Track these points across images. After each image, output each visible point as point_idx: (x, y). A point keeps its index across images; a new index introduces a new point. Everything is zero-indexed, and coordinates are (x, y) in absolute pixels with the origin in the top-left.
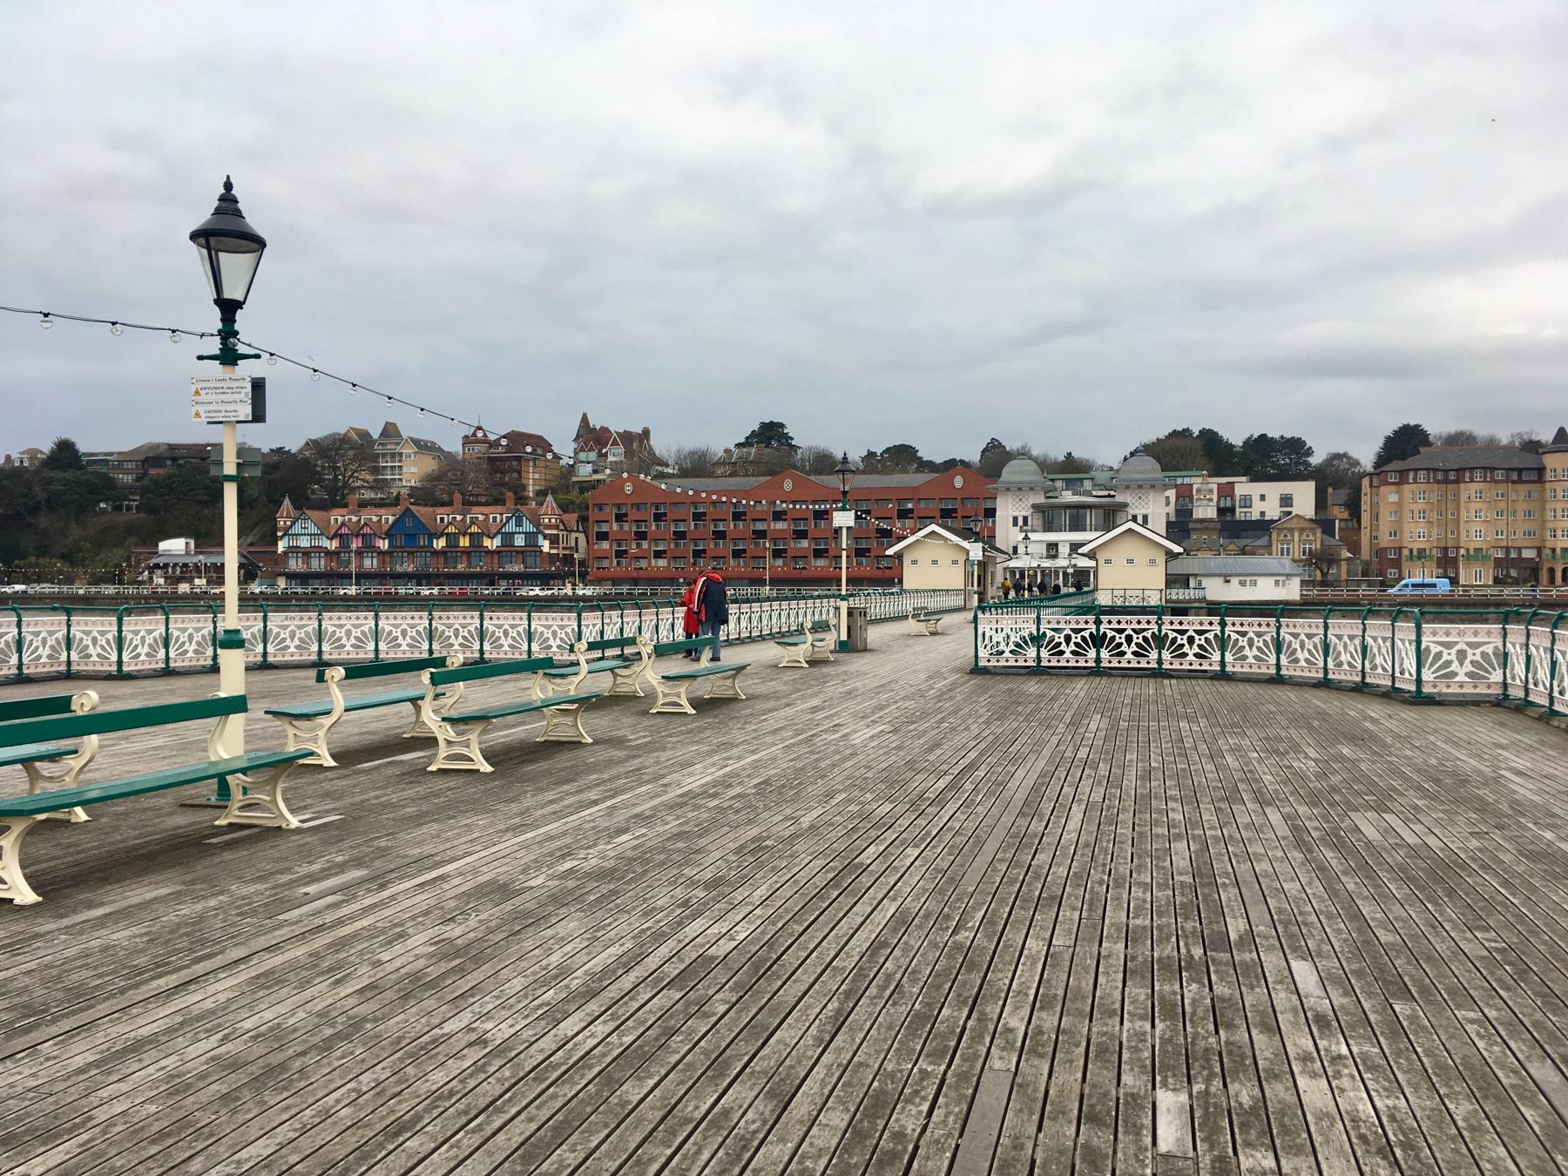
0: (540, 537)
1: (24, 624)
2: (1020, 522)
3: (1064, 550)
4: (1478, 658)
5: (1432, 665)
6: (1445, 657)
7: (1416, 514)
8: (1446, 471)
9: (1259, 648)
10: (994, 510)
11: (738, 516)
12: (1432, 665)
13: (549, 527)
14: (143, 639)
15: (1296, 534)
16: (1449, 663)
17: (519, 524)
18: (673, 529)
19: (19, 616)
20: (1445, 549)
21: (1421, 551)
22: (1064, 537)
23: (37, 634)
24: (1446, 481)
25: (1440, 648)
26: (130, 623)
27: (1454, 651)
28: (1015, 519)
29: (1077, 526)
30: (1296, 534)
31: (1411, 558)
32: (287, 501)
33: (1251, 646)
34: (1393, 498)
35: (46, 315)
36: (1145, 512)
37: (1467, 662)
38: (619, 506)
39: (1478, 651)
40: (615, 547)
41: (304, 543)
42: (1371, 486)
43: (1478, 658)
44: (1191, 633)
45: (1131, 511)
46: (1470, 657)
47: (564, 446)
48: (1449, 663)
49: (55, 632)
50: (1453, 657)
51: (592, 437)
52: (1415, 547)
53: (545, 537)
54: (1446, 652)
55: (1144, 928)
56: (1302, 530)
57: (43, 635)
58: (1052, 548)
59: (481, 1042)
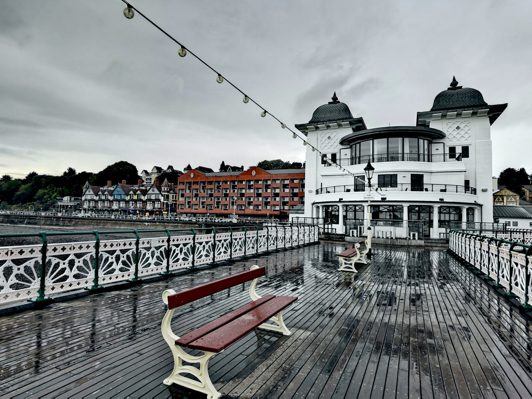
4: (22, 271)
5: (52, 273)
6: (61, 266)
9: (57, 265)
12: (52, 273)
13: (164, 192)
14: (181, 249)
16: (63, 270)
25: (58, 260)
27: (114, 256)
32: (166, 180)
33: (181, 252)
37: (75, 268)
39: (22, 267)
40: (248, 200)
41: (153, 197)
43: (22, 271)
44: (118, 252)
45: (449, 142)
46: (77, 264)
47: (216, 169)
48: (63, 270)
49: (227, 240)
50: (66, 265)
51: (224, 168)
53: (162, 195)
54: (62, 262)
57: (181, 246)
59: (499, 327)
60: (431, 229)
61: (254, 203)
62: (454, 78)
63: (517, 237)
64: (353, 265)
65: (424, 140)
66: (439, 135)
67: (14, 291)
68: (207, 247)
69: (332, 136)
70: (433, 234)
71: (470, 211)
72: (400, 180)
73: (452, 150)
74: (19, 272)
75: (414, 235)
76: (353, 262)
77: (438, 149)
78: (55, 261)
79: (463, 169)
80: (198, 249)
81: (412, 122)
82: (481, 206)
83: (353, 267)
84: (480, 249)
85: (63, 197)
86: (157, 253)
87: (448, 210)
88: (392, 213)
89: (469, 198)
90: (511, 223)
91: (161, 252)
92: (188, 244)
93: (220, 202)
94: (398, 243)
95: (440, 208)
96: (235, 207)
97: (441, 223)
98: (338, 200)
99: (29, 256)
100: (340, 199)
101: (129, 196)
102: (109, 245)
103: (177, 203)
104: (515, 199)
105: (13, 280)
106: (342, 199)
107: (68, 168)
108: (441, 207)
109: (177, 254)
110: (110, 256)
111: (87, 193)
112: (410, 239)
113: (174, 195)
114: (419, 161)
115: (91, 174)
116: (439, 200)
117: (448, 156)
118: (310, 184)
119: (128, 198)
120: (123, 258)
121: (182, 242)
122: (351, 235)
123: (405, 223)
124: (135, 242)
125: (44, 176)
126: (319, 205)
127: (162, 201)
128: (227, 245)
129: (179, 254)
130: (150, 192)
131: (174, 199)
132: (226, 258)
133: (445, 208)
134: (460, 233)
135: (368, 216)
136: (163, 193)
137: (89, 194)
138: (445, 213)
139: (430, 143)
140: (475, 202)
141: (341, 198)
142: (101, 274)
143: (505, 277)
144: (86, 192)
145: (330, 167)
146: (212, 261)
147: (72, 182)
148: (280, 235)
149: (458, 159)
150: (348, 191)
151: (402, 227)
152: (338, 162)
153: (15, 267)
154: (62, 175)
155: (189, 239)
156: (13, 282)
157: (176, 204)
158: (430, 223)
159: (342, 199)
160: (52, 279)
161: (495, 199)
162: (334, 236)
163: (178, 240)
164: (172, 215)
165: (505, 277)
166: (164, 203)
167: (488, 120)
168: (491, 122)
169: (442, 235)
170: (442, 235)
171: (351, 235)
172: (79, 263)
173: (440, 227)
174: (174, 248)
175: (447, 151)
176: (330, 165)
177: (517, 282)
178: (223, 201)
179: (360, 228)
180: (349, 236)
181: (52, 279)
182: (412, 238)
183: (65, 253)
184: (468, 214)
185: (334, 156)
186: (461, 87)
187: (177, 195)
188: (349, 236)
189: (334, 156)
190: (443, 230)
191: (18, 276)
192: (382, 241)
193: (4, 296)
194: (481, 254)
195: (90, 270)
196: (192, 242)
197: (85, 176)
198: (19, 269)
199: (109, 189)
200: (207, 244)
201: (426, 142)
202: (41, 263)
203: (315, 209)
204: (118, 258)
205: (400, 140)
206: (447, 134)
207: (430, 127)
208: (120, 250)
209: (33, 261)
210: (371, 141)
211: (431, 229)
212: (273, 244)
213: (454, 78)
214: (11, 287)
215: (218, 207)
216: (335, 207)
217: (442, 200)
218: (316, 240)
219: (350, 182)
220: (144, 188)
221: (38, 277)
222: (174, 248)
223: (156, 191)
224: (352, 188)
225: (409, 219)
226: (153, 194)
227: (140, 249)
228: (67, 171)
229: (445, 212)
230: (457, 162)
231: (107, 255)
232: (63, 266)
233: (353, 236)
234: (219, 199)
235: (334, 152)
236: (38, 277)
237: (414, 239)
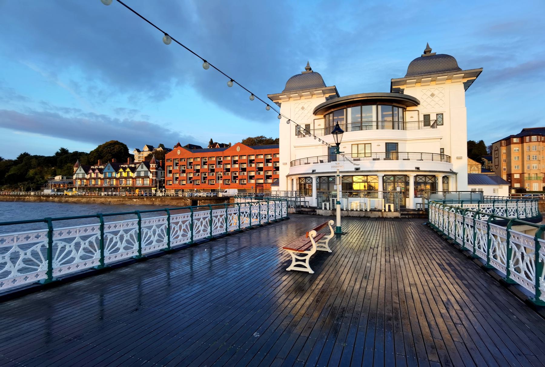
0: (149, 172)
1: (142, 222)
9: (64, 248)
10: (278, 167)
13: (153, 169)
14: (180, 226)
16: (70, 252)
17: (142, 168)
19: (140, 218)
23: (116, 233)
25: (64, 243)
26: (146, 221)
33: (154, 234)
35: (232, 80)
39: (29, 251)
43: (29, 256)
45: (423, 109)
46: (82, 246)
48: (70, 252)
50: (73, 247)
53: (151, 172)
57: (154, 227)
60: (407, 199)
61: (239, 178)
62: (428, 44)
66: (414, 102)
67: (22, 274)
68: (184, 227)
69: (305, 106)
71: (446, 179)
73: (427, 118)
74: (26, 257)
75: (389, 206)
77: (411, 115)
78: (60, 245)
79: (439, 136)
80: (196, 226)
81: (385, 90)
82: (456, 174)
83: (307, 264)
85: (55, 176)
86: (502, 211)
88: (366, 184)
89: (443, 166)
91: (186, 226)
92: (187, 221)
93: (206, 177)
94: (351, 214)
96: (221, 182)
98: (311, 172)
99: (36, 241)
100: (313, 171)
101: (119, 174)
102: (112, 226)
103: (166, 179)
105: (20, 264)
107: (60, 148)
108: (417, 175)
109: (177, 231)
110: (115, 237)
111: (78, 172)
112: (385, 211)
113: (163, 171)
114: (393, 128)
115: (82, 154)
116: (414, 169)
117: (422, 124)
118: (284, 155)
119: (118, 175)
120: (127, 237)
121: (486, 207)
122: (323, 209)
123: (380, 195)
124: (137, 222)
125: (36, 157)
126: (293, 177)
127: (151, 177)
128: (207, 223)
129: (179, 231)
130: (139, 169)
131: (163, 176)
132: (206, 236)
133: (421, 177)
135: (338, 188)
136: (152, 170)
137: (79, 172)
139: (404, 110)
140: (451, 170)
141: (314, 169)
142: (106, 253)
144: (77, 170)
145: (304, 138)
146: (190, 241)
147: (64, 161)
148: (255, 211)
149: (433, 127)
150: (322, 162)
151: (377, 197)
152: (312, 132)
153: (22, 253)
154: (54, 155)
155: (188, 217)
156: (20, 267)
157: (164, 180)
158: (405, 193)
160: (59, 262)
161: (471, 168)
162: (307, 210)
163: (177, 218)
164: (161, 191)
166: (152, 179)
171: (323, 209)
172: (84, 244)
173: (416, 196)
174: (496, 209)
175: (422, 118)
176: (304, 136)
178: (210, 176)
179: (333, 200)
180: (321, 208)
181: (59, 262)
182: (387, 210)
183: (71, 236)
184: (443, 182)
187: (166, 171)
188: (321, 208)
189: (308, 126)
190: (420, 200)
191: (25, 261)
192: (355, 214)
193: (13, 280)
195: (96, 251)
196: (190, 219)
197: (77, 155)
198: (26, 254)
199: (100, 167)
200: (184, 224)
202: (48, 247)
203: (290, 182)
204: (122, 238)
205: (374, 107)
207: (404, 93)
208: (124, 230)
209: (39, 246)
211: (407, 199)
212: (265, 218)
213: (428, 44)
214: (20, 271)
215: (205, 182)
216: (309, 179)
217: (418, 168)
218: (285, 215)
219: (323, 152)
220: (133, 166)
221: (46, 260)
222: (496, 209)
223: (145, 168)
224: (326, 159)
225: (383, 190)
226: (142, 170)
227: (105, 234)
228: (59, 151)
230: (432, 129)
231: (112, 236)
232: (70, 249)
233: (325, 209)
234: (205, 175)
235: (307, 123)
236: (46, 260)
237: (390, 210)
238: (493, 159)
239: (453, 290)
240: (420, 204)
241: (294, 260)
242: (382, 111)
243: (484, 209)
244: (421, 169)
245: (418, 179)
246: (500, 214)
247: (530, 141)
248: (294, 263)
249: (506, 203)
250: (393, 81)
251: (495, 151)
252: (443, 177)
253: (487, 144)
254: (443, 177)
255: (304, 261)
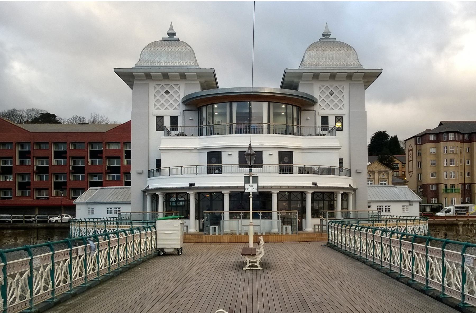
2: (167, 122)
3: (230, 160)
7: (449, 162)
8: (464, 134)
11: (94, 155)
15: (376, 175)
18: (107, 164)
20: (464, 185)
21: (453, 186)
22: (232, 143)
24: (463, 141)
28: (160, 119)
29: (246, 126)
30: (376, 175)
31: (446, 191)
34: (433, 151)
36: (338, 112)
38: (22, 144)
42: (416, 144)
45: (321, 110)
52: (449, 183)
55: (246, 113)
56: (380, 171)
58: (214, 161)
60: (303, 220)
63: (392, 225)
64: (258, 262)
65: (293, 106)
70: (306, 227)
71: (345, 196)
72: (266, 159)
76: (258, 260)
83: (258, 265)
84: (373, 241)
87: (321, 196)
90: (384, 208)
95: (313, 194)
97: (315, 214)
104: (388, 175)
106: (194, 184)
116: (312, 185)
134: (339, 224)
138: (318, 200)
143: (396, 264)
159: (194, 184)
165: (396, 264)
167: (364, 87)
168: (366, 87)
169: (317, 227)
170: (317, 227)
174: (399, 228)
175: (319, 123)
177: (405, 265)
184: (342, 200)
185: (174, 120)
186: (334, 40)
190: (317, 221)
194: (374, 246)
200: (21, 277)
201: (295, 109)
205: (265, 105)
206: (319, 101)
210: (228, 105)
222: (399, 228)
229: (318, 198)
238: (407, 162)
239: (315, 203)
240: (318, 225)
241: (248, 262)
242: (274, 108)
243: (390, 227)
244: (318, 185)
245: (315, 196)
246: (410, 232)
247: (448, 140)
248: (248, 265)
249: (406, 221)
250: (287, 71)
251: (409, 151)
252: (342, 194)
253: (401, 138)
254: (342, 194)
255: (256, 262)
